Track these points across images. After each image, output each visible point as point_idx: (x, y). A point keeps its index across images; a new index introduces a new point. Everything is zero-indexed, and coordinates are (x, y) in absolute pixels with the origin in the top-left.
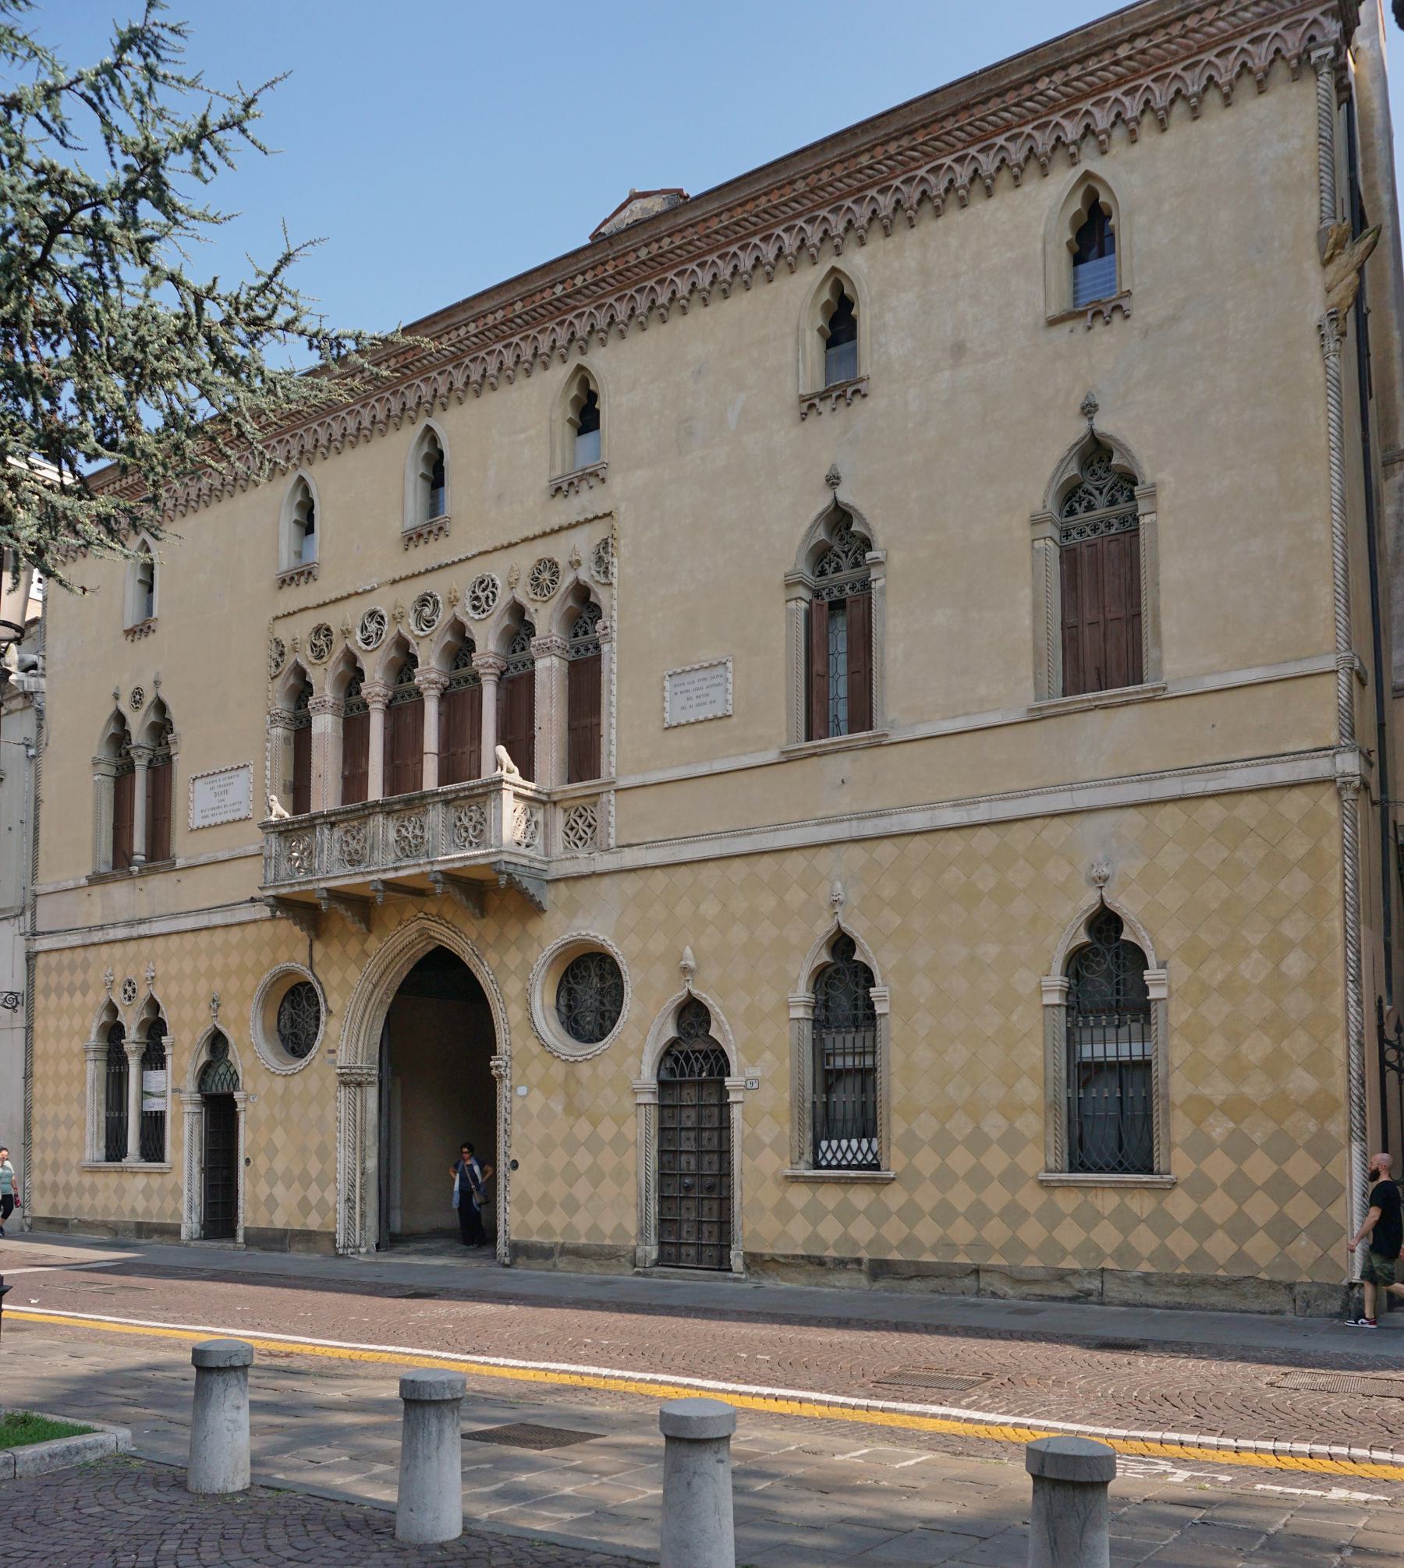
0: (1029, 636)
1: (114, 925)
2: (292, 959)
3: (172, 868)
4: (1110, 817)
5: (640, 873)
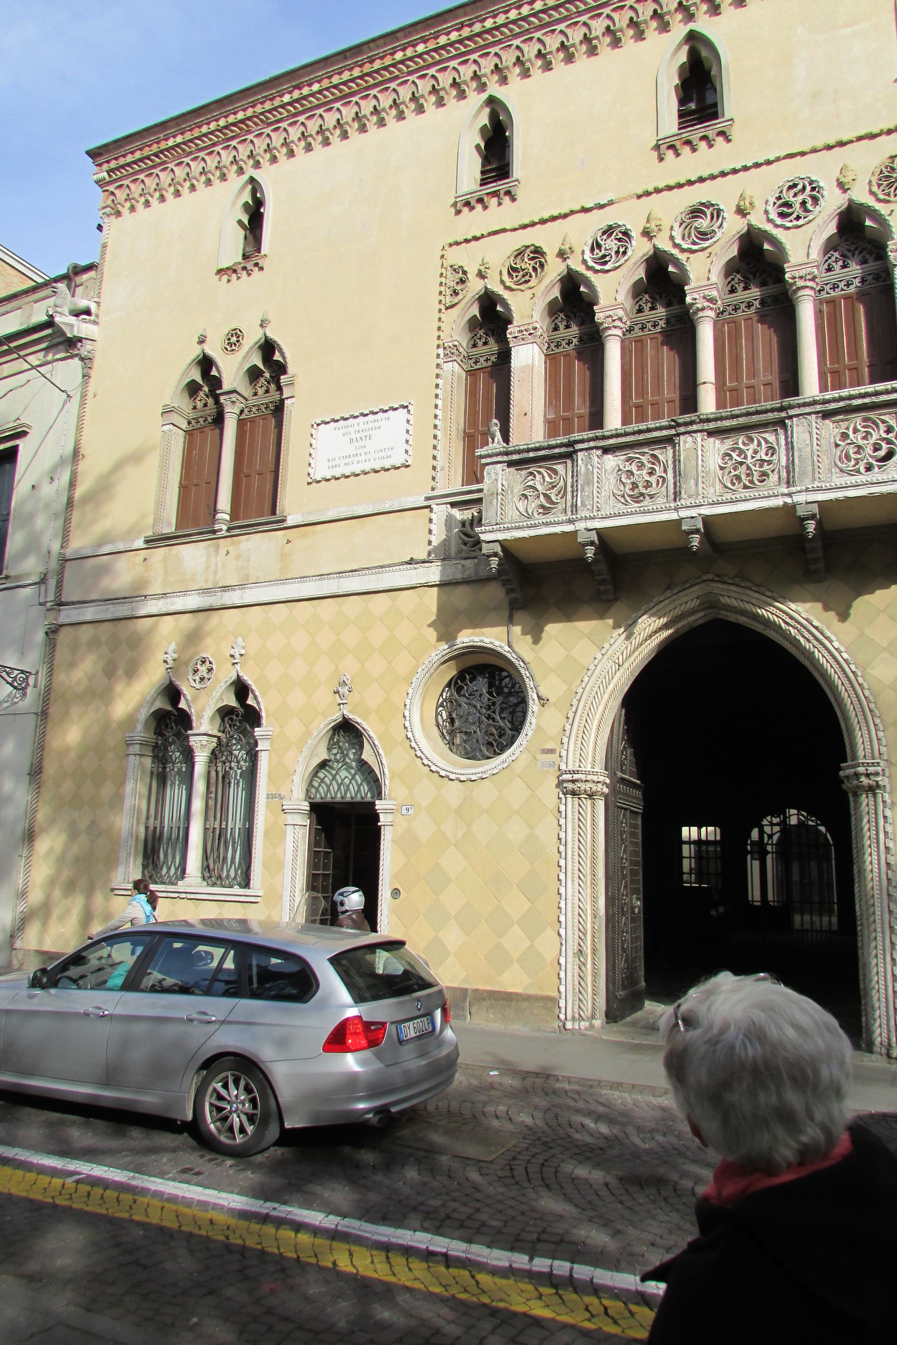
1: (185, 593)
3: (279, 524)
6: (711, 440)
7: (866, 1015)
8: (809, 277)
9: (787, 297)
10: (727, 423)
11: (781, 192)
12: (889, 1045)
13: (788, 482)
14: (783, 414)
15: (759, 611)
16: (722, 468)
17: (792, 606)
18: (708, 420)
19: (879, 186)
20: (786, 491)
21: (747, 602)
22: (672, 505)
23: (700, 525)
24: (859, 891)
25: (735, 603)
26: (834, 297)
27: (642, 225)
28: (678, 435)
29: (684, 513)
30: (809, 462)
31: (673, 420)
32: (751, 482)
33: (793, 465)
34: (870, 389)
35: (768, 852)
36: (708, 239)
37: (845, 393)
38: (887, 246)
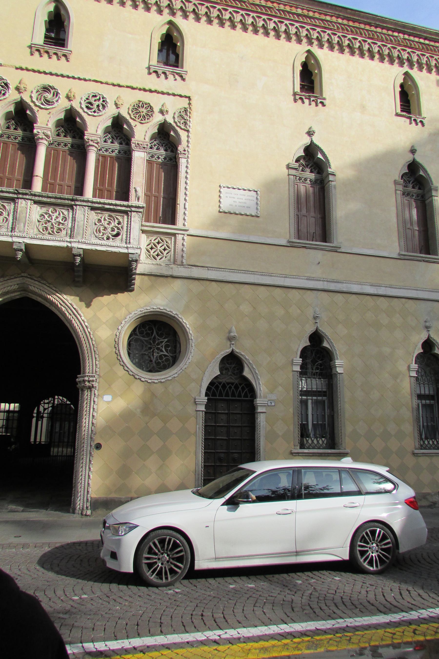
0: (396, 226)
4: (430, 303)
5: (201, 282)
6: (36, 206)
7: (74, 496)
8: (95, 141)
9: (84, 147)
10: (45, 200)
11: (89, 97)
12: (83, 509)
13: (70, 236)
14: (73, 203)
15: (48, 296)
16: (39, 221)
17: (65, 296)
18: (35, 195)
19: (132, 111)
20: (69, 240)
21: (43, 291)
22: (10, 234)
23: (23, 248)
24: (78, 436)
25: (37, 290)
26: (105, 155)
27: (16, 84)
28: (18, 198)
29: (15, 239)
30: (82, 229)
31: (16, 190)
32: (53, 232)
33: (74, 228)
34: (114, 202)
35: (34, 417)
36: (50, 105)
37: (102, 201)
38: (131, 140)
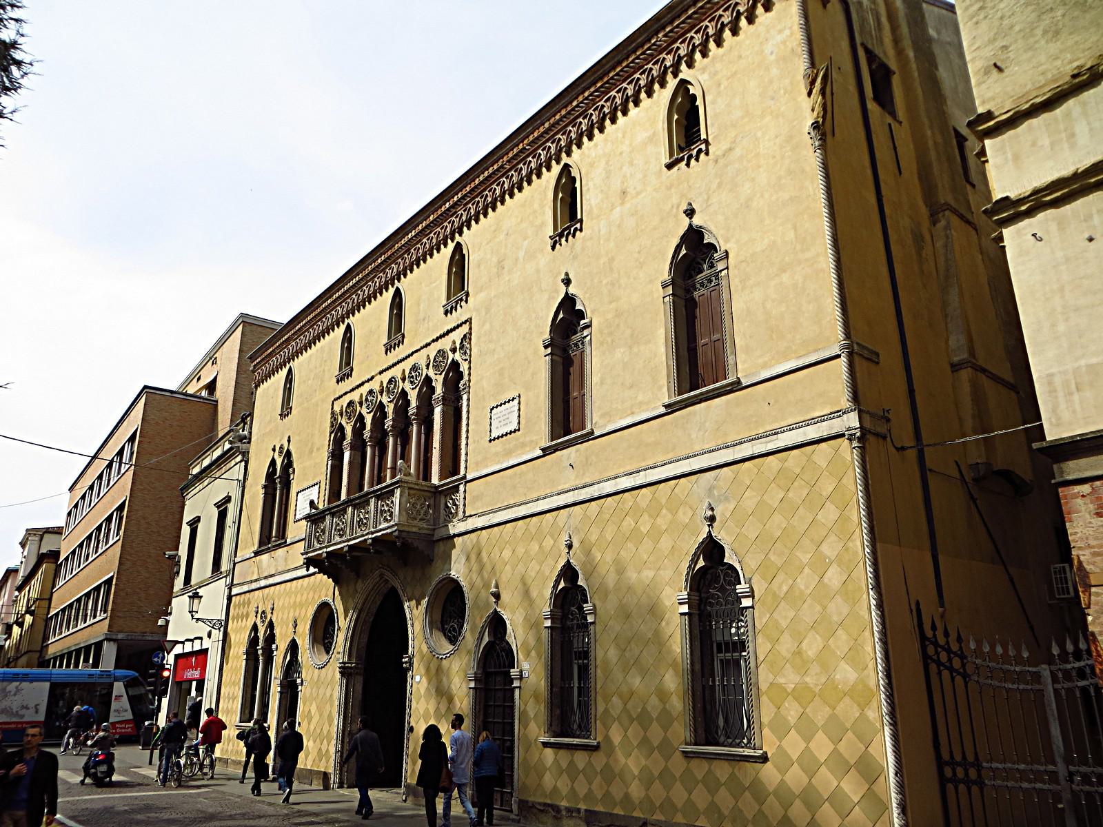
2: (326, 596)
